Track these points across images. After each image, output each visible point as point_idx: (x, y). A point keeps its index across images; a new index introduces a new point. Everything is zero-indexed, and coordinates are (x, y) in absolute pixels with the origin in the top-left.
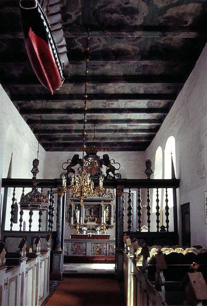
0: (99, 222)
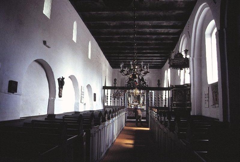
0: (139, 103)
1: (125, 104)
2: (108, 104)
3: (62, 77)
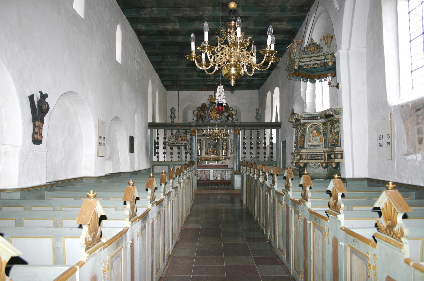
1: (191, 158)
2: (160, 157)
3: (41, 92)
